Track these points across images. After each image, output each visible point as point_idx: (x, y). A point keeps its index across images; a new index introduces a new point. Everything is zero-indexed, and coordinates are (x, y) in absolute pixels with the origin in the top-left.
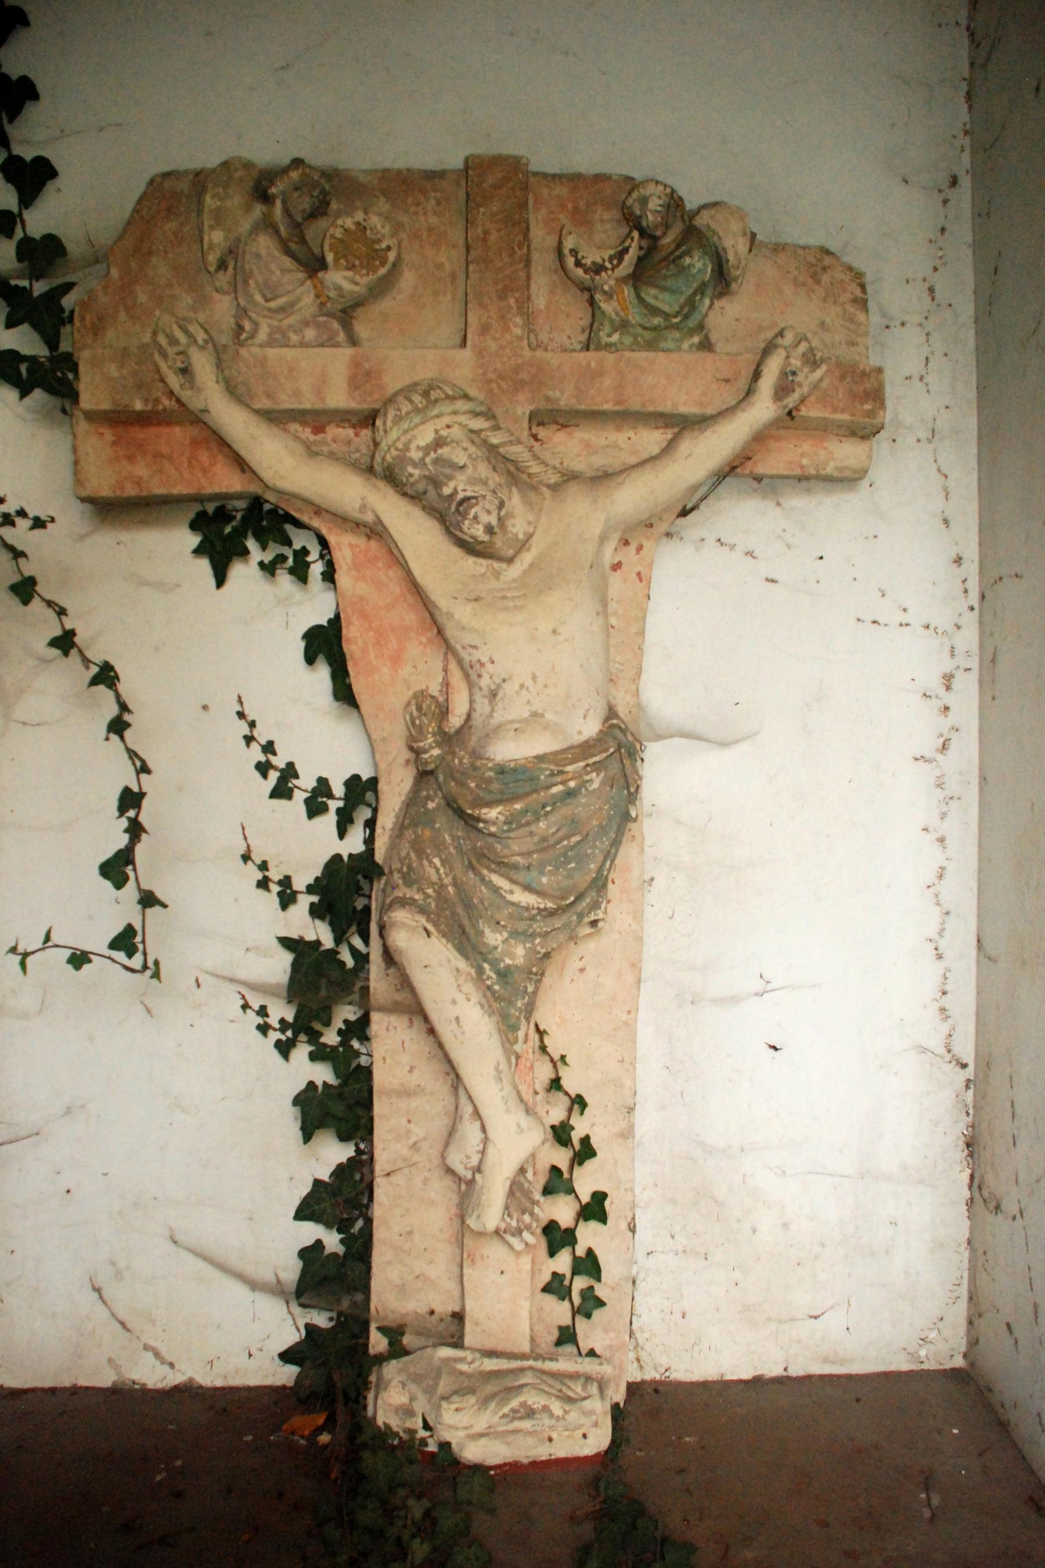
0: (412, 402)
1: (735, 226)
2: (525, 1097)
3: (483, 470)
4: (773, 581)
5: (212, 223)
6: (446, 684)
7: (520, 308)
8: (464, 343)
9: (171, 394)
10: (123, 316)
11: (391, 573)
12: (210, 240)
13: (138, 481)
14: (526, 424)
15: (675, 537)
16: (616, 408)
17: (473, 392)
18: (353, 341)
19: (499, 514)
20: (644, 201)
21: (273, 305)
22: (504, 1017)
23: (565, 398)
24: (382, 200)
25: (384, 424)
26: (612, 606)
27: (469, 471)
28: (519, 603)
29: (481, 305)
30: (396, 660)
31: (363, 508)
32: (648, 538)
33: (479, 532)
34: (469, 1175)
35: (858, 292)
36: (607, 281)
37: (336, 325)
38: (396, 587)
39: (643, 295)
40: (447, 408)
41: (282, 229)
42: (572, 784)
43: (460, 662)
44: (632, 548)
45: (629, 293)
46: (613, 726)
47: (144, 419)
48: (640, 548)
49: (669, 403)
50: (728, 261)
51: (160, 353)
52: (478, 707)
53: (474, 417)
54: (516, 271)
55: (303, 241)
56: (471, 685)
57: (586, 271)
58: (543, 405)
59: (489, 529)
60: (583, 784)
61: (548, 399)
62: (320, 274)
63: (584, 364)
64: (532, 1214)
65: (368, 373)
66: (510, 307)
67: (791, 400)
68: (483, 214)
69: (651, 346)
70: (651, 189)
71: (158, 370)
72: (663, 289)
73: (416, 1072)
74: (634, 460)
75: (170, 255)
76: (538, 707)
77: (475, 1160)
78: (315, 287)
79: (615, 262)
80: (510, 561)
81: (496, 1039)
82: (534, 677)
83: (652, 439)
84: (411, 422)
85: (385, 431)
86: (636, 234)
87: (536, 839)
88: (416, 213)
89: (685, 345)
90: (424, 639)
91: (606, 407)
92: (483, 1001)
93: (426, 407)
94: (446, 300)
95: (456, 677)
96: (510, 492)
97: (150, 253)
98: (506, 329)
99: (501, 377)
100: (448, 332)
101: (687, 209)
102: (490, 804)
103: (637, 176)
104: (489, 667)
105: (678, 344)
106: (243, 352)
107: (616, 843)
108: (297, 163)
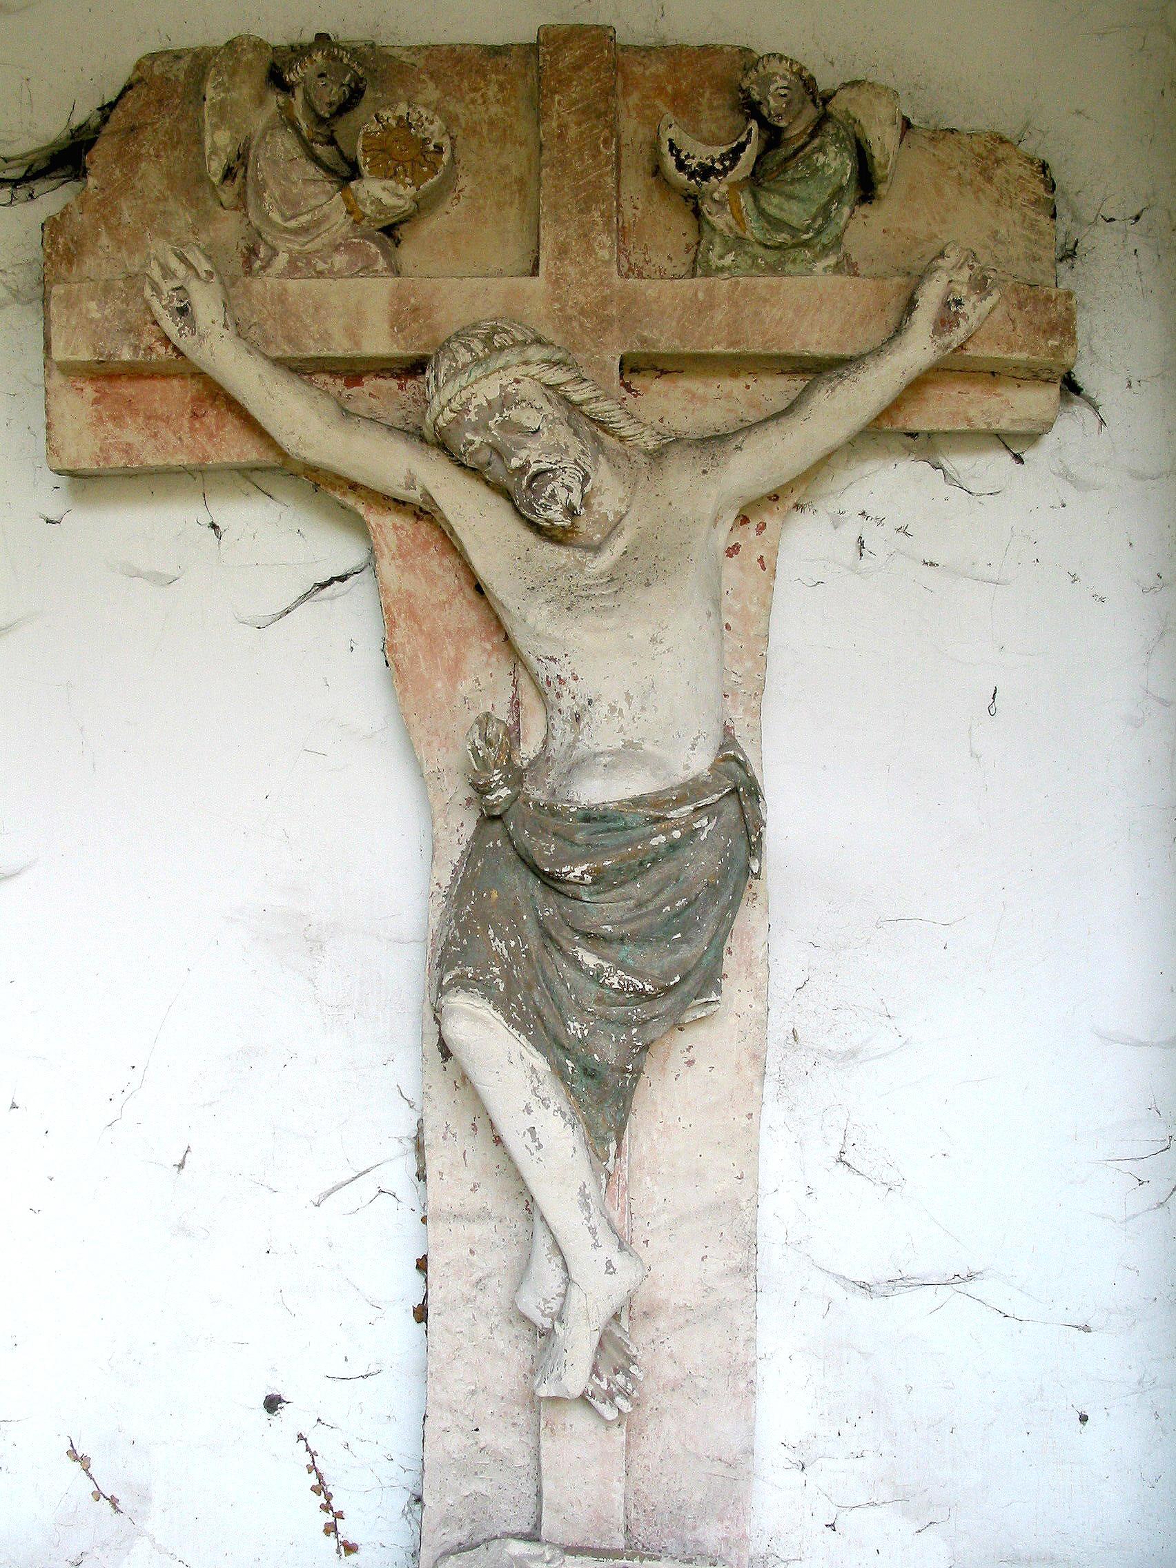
0: (471, 350)
1: (883, 111)
2: (617, 1224)
3: (564, 435)
4: (932, 564)
5: (215, 120)
6: (516, 704)
7: (608, 223)
8: (534, 272)
9: (166, 340)
10: (104, 240)
11: (446, 562)
12: (214, 143)
13: (127, 449)
14: (616, 372)
15: (807, 510)
16: (731, 350)
17: (548, 333)
18: (396, 271)
19: (582, 491)
20: (766, 81)
21: (292, 224)
22: (590, 1127)
23: (665, 341)
24: (431, 85)
25: (436, 378)
26: (728, 601)
27: (544, 436)
28: (609, 604)
29: (558, 220)
30: (455, 671)
31: (411, 483)
32: (772, 513)
33: (556, 515)
34: (547, 1323)
35: (1041, 191)
36: (718, 187)
37: (374, 249)
38: (451, 579)
39: (765, 206)
40: (511, 357)
41: (304, 125)
42: (677, 834)
43: (533, 678)
44: (753, 525)
45: (746, 202)
46: (727, 759)
47: (135, 372)
48: (761, 528)
49: (797, 343)
50: (873, 157)
51: (153, 289)
52: (558, 733)
53: (596, 553)
54: (601, 176)
55: (331, 141)
56: (547, 705)
57: (692, 175)
58: (637, 348)
59: (570, 511)
60: (694, 833)
61: (644, 341)
62: (353, 185)
63: (690, 294)
64: (627, 1373)
65: (415, 309)
66: (595, 223)
67: (958, 335)
68: (559, 102)
69: (774, 269)
70: (774, 66)
71: (149, 309)
72: (790, 197)
73: (480, 1190)
74: (753, 417)
75: (163, 161)
76: (634, 735)
77: (555, 1306)
78: (347, 201)
79: (727, 163)
80: (597, 549)
81: (582, 1153)
82: (628, 698)
83: (776, 390)
84: (469, 376)
85: (437, 386)
86: (754, 125)
87: (631, 903)
88: (473, 101)
89: (820, 266)
90: (489, 647)
91: (717, 349)
92: (566, 1109)
93: (487, 357)
94: (512, 212)
95: (528, 697)
96: (596, 461)
97: (138, 157)
98: (589, 251)
99: (583, 312)
100: (515, 255)
101: (820, 90)
102: (574, 861)
103: (760, 51)
104: (572, 684)
105: (809, 266)
106: (257, 286)
107: (733, 906)
108: (322, 39)
